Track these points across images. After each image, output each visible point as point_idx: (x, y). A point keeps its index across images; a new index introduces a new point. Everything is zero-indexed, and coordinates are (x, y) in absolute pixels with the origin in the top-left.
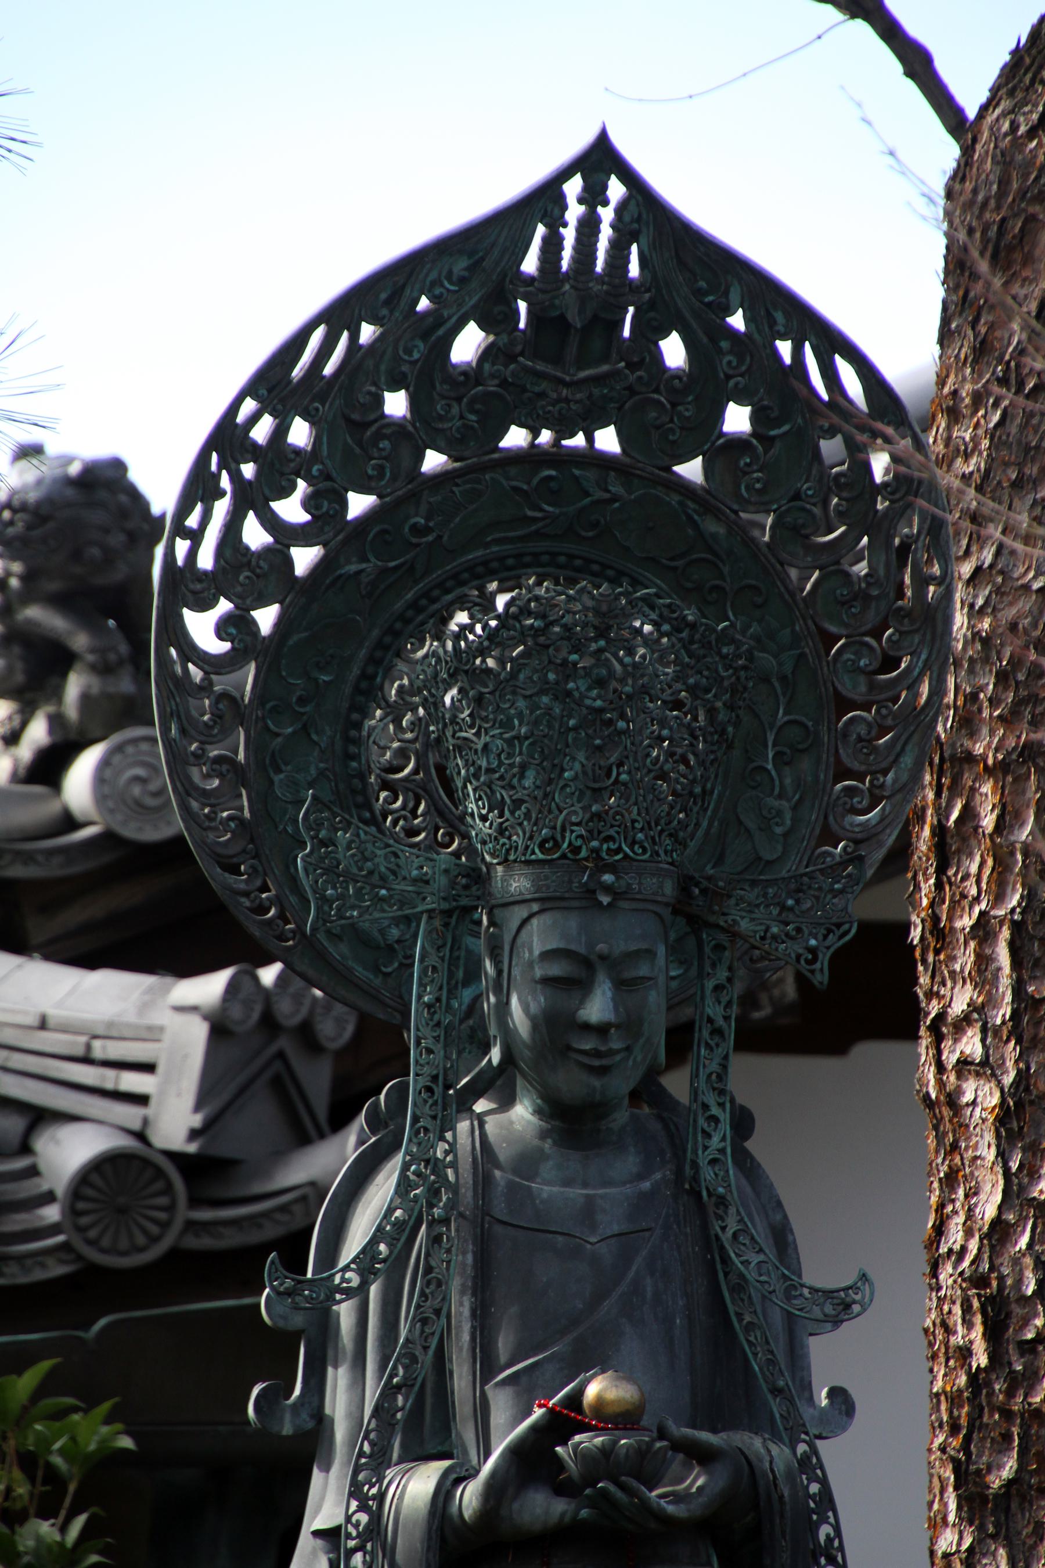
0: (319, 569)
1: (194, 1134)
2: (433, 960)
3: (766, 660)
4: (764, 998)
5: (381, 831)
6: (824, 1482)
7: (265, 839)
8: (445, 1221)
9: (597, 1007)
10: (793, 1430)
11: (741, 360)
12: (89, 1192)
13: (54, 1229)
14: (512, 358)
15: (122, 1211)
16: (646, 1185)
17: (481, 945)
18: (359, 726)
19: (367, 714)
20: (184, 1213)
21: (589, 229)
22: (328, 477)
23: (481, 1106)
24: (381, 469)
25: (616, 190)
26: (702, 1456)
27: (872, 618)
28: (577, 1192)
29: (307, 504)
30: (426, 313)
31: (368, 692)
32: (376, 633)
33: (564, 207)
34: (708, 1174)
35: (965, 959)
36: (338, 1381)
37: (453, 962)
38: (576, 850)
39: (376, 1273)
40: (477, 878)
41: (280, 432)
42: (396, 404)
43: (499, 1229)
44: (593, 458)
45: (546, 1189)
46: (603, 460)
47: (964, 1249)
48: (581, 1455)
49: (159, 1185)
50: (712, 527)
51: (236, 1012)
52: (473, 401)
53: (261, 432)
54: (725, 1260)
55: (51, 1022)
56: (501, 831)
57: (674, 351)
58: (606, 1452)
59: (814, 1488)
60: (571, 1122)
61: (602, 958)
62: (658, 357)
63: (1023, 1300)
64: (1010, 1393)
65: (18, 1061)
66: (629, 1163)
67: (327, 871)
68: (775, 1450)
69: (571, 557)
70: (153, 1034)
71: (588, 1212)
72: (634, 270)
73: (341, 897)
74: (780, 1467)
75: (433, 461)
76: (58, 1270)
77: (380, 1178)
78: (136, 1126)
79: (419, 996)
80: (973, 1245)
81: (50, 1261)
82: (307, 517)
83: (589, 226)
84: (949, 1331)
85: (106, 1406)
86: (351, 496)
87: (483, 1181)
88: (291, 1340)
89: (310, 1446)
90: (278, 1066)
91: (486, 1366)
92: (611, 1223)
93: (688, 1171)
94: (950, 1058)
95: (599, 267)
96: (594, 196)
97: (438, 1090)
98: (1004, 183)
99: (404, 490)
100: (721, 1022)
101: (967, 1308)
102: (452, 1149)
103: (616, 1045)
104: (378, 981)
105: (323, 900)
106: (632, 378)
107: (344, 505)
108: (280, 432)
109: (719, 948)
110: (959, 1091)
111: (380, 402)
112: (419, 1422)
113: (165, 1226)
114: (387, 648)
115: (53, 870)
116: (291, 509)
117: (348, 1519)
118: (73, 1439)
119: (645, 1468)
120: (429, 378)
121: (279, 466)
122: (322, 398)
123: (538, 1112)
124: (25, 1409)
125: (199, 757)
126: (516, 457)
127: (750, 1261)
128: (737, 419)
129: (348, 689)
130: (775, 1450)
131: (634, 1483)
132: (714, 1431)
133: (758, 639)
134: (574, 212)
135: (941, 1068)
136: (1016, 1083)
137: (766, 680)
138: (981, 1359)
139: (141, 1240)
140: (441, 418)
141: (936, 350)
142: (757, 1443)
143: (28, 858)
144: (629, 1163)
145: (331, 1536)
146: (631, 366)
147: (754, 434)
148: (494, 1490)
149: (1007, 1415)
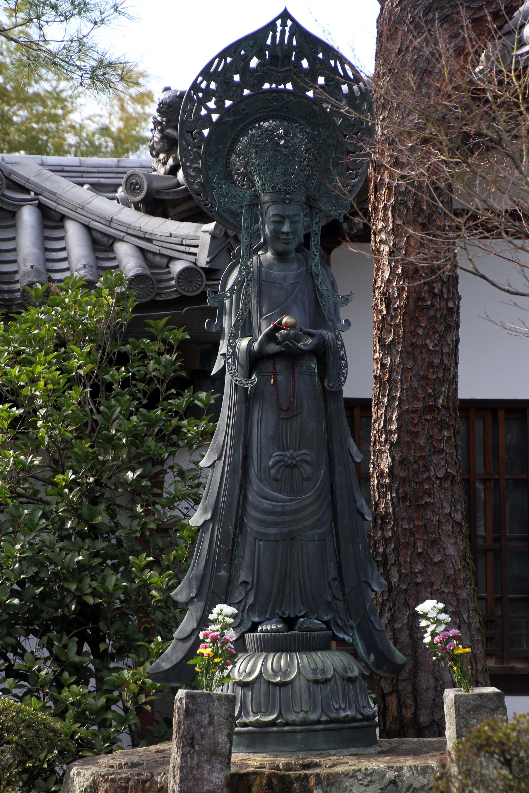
0: (219, 120)
1: (208, 263)
2: (247, 217)
3: (330, 141)
4: (355, 228)
5: (235, 186)
6: (342, 341)
7: (206, 186)
8: (250, 280)
9: (286, 228)
10: (334, 329)
11: (321, 65)
12: (182, 277)
13: (173, 286)
14: (265, 66)
15: (190, 282)
16: (299, 271)
17: (258, 213)
18: (229, 159)
19: (231, 156)
20: (205, 282)
21: (283, 33)
22: (220, 97)
23: (260, 253)
24: (233, 94)
25: (289, 23)
26: (311, 335)
27: (355, 130)
28: (282, 273)
29: (215, 103)
30: (243, 55)
31: (231, 150)
32: (233, 136)
33: (277, 27)
34: (314, 268)
35: (381, 216)
36: (226, 319)
37: (252, 217)
38: (280, 189)
39: (234, 293)
40: (257, 197)
41: (208, 85)
42: (237, 78)
43: (263, 282)
44: (285, 91)
45: (274, 273)
46: (288, 91)
47: (381, 286)
48: (282, 335)
49: (199, 275)
50: (316, 108)
51: (218, 232)
52: (256, 77)
53: (203, 85)
54: (318, 289)
55: (173, 235)
56: (262, 185)
57: (305, 63)
58: (287, 334)
59: (340, 343)
60: (281, 256)
61: (287, 216)
62: (301, 65)
63: (395, 298)
64: (391, 320)
65: (165, 245)
66: (295, 266)
67: (221, 195)
68: (329, 334)
69: (281, 116)
70: (197, 238)
71: (285, 278)
72: (294, 43)
73: (224, 202)
74: (330, 338)
75: (246, 92)
76: (175, 296)
77: (235, 270)
78: (194, 261)
79: (244, 226)
80: (383, 285)
81: (173, 294)
82: (215, 107)
83: (283, 32)
84: (377, 306)
85: (183, 328)
86: (226, 101)
87: (259, 271)
88: (215, 309)
89: (220, 334)
90: (229, 246)
91: (261, 315)
92: (291, 280)
93: (309, 268)
94: (378, 240)
95: (286, 42)
96: (284, 24)
97: (248, 249)
98: (390, 19)
99: (239, 100)
100: (317, 231)
101: (381, 301)
102: (252, 263)
103: (291, 237)
104: (235, 222)
105: (220, 203)
106: (295, 70)
107: (224, 104)
108: (208, 85)
109: (317, 213)
110: (380, 248)
111: (232, 77)
112: (245, 328)
113: (201, 285)
114: (236, 139)
115: (174, 197)
116: (211, 105)
117: (228, 351)
118: (175, 336)
119: (297, 338)
120: (245, 71)
121: (208, 94)
122: (218, 77)
123: (273, 254)
124: (163, 328)
125: (190, 167)
126: (267, 91)
127: (325, 289)
128: (321, 80)
129: (227, 150)
130: (329, 334)
131: (294, 342)
132: (315, 329)
133: (327, 136)
134: (279, 28)
135: (376, 242)
136: (393, 245)
137: (330, 146)
138: (384, 312)
139: (195, 289)
140: (248, 81)
141: (375, 62)
142: (325, 332)
143: (168, 194)
144: (295, 266)
145: (224, 355)
146: (294, 67)
147: (325, 84)
148: (261, 344)
149: (391, 325)
